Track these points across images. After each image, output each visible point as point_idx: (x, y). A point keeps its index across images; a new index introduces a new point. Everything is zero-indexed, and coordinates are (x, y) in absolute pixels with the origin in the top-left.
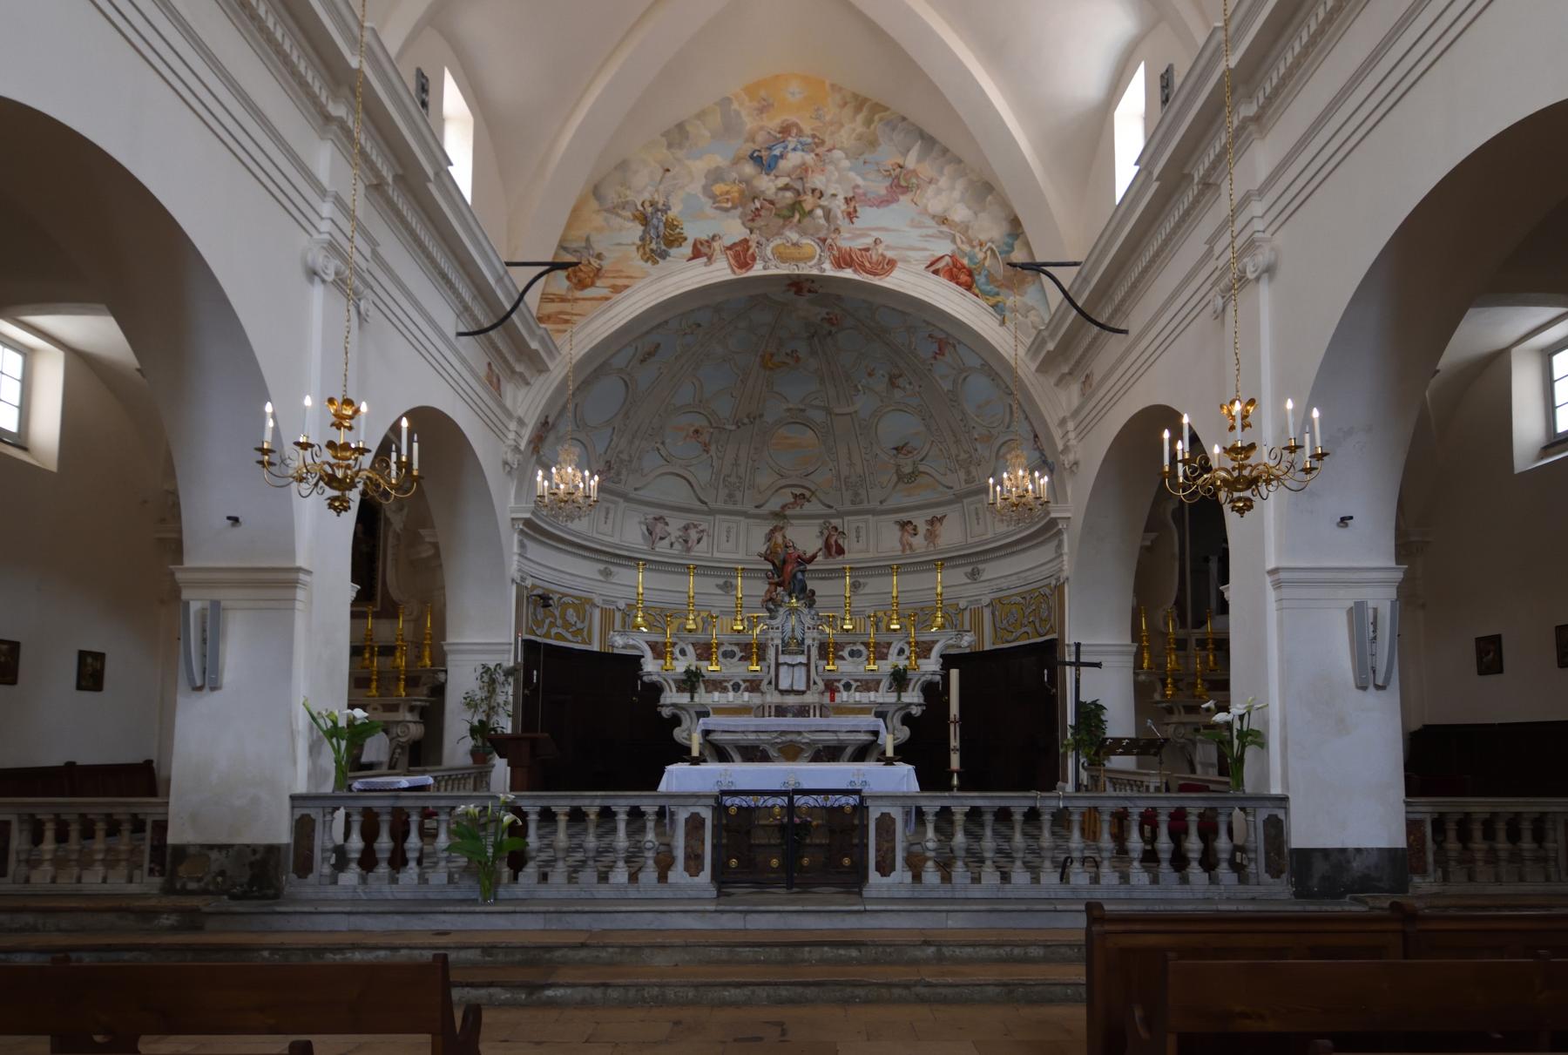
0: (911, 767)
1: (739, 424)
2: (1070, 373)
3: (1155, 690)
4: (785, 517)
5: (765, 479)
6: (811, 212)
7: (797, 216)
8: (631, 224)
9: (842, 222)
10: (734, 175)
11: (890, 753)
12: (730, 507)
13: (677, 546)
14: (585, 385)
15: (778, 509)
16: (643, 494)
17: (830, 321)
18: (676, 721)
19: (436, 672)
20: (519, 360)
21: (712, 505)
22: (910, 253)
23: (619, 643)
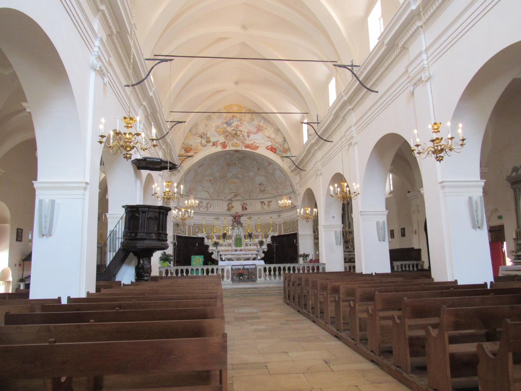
1: (221, 178)
5: (227, 191)
9: (247, 138)
18: (212, 253)
23: (200, 235)
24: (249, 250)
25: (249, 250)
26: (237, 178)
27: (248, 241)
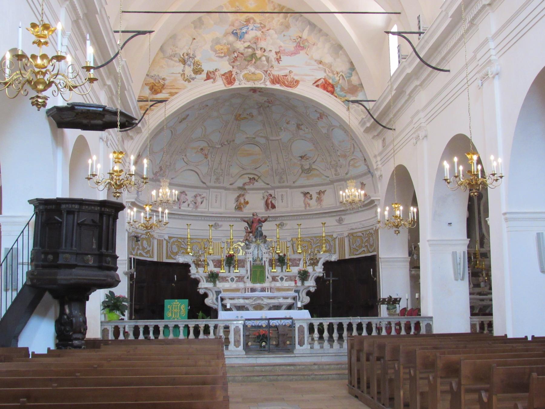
0: (307, 311)
1: (222, 145)
2: (378, 135)
4: (245, 189)
5: (235, 170)
6: (260, 58)
7: (254, 60)
8: (177, 64)
9: (275, 63)
10: (225, 41)
12: (218, 185)
13: (191, 205)
15: (241, 185)
17: (269, 102)
18: (206, 295)
21: (209, 184)
23: (181, 259)
25: (279, 289)
26: (256, 144)
27: (277, 270)
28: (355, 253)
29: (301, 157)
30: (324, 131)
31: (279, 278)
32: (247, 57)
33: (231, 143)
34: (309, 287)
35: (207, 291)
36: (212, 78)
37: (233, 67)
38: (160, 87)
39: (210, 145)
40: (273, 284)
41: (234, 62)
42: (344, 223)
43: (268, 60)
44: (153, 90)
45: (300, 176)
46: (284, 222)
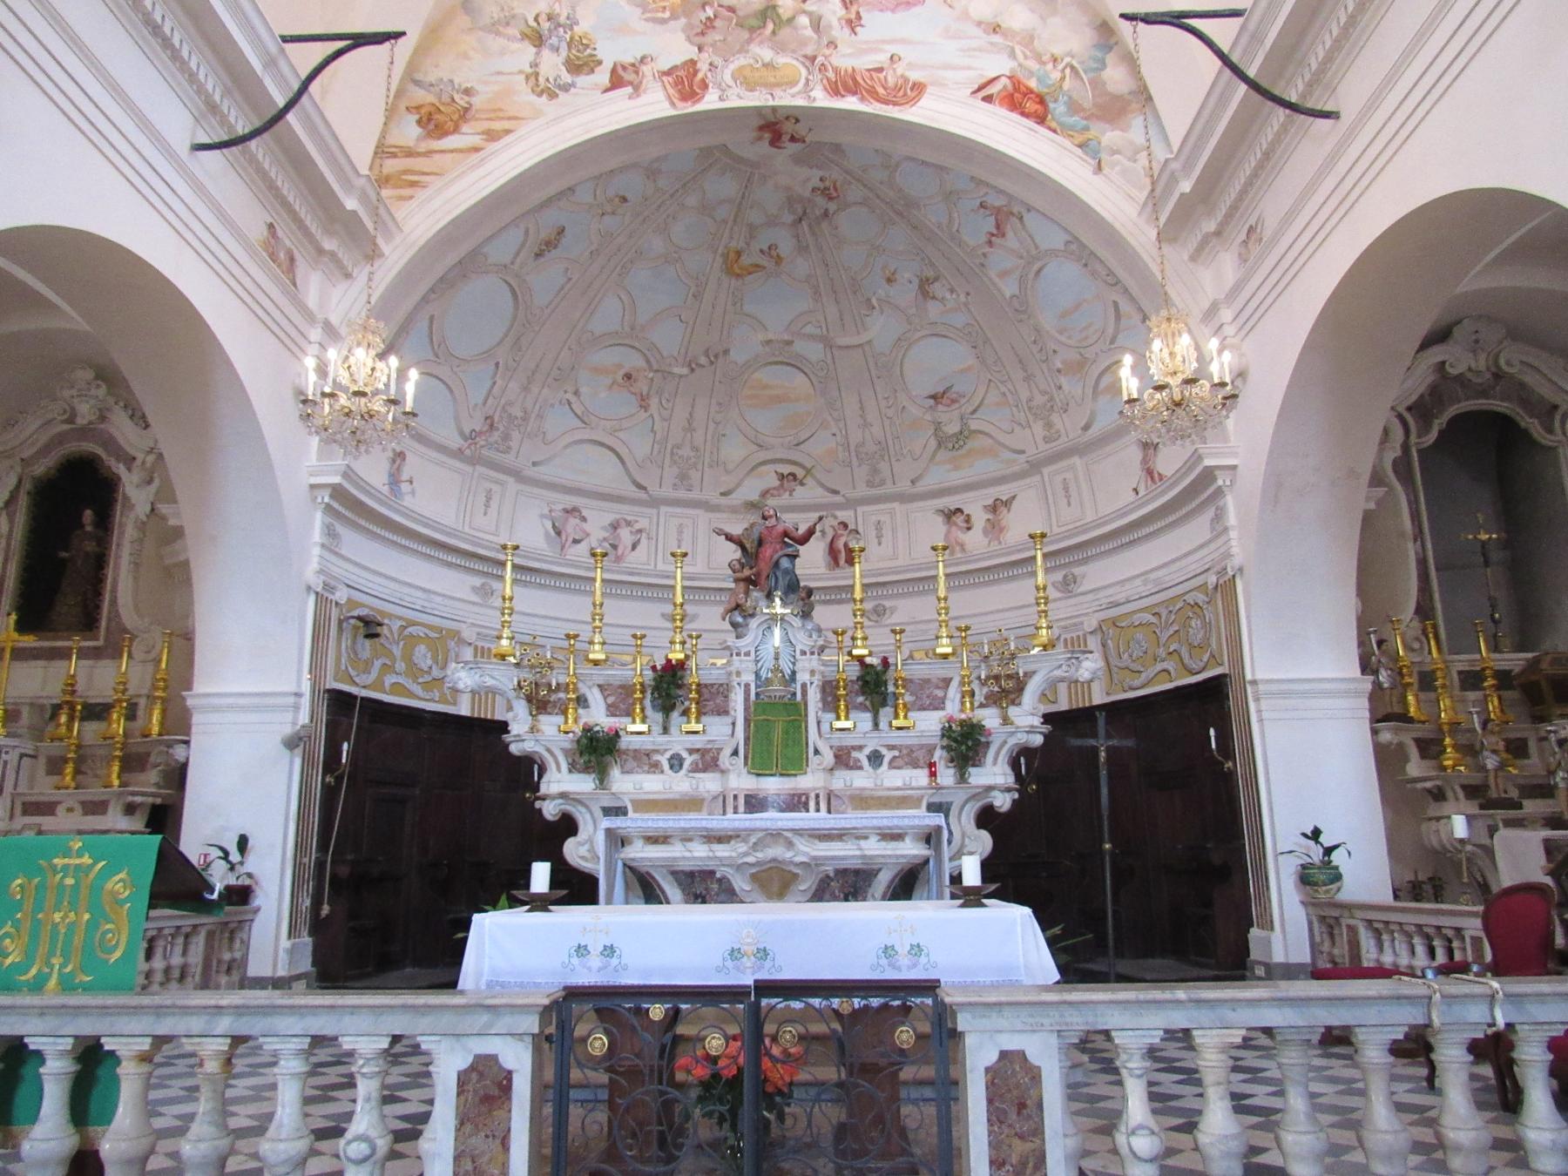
2: (1218, 233)
3: (1406, 759)
5: (735, 450)
6: (791, 20)
7: (770, 26)
8: (516, 46)
9: (840, 33)
11: (972, 875)
12: (682, 494)
14: (446, 284)
15: (754, 497)
16: (546, 472)
17: (825, 192)
19: (170, 745)
20: (329, 232)
22: (949, 74)
24: (862, 801)
25: (862, 801)
26: (796, 364)
27: (856, 725)
28: (1128, 682)
29: (934, 397)
30: (1009, 288)
31: (862, 757)
32: (747, 16)
33: (721, 359)
34: (990, 788)
35: (569, 808)
36: (631, 83)
37: (700, 49)
38: (455, 117)
39: (655, 367)
40: (844, 780)
41: (703, 34)
42: (1081, 589)
43: (816, 24)
44: (431, 127)
45: (933, 456)
46: (887, 604)
